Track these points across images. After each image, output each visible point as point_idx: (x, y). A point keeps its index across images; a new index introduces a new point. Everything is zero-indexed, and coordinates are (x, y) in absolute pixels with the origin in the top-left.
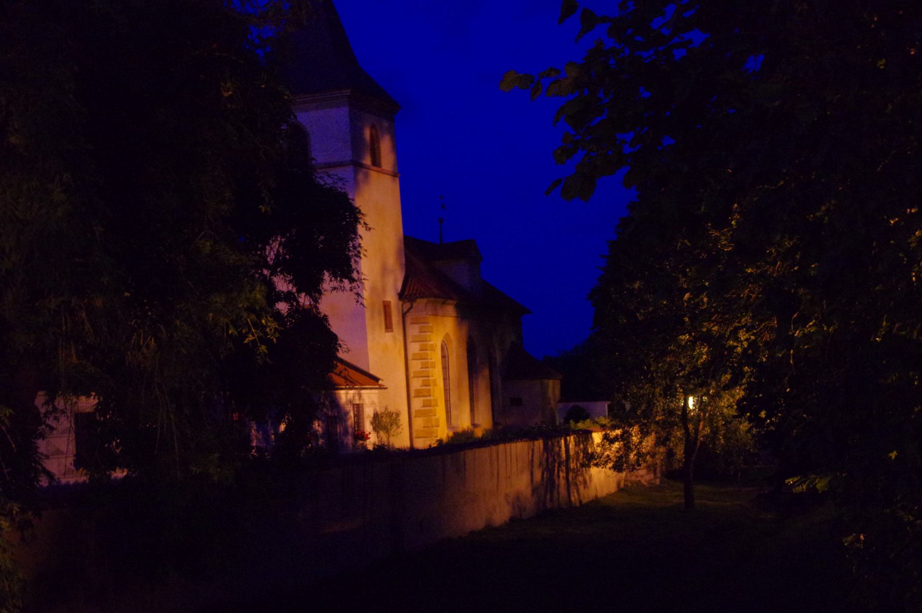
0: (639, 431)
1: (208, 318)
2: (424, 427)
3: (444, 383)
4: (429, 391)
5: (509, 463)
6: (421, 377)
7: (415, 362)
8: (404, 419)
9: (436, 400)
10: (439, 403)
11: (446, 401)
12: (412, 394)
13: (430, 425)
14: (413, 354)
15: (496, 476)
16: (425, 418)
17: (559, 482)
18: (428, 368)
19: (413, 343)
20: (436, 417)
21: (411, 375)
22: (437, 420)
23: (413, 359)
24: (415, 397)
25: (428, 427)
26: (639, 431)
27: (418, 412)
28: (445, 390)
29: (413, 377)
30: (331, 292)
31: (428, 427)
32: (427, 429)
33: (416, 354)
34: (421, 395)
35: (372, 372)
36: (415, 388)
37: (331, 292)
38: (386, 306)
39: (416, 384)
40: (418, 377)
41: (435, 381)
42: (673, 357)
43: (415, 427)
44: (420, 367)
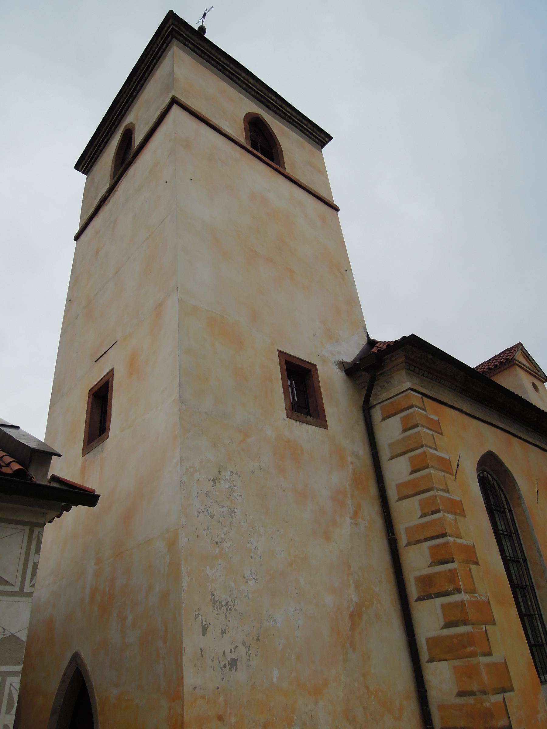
0: (356, 602)
1: (450, 551)
2: (461, 694)
4: (452, 576)
6: (426, 540)
7: (405, 503)
10: (497, 612)
12: (413, 591)
13: (475, 687)
14: (398, 486)
16: (457, 663)
18: (437, 511)
19: (392, 461)
20: (495, 658)
23: (400, 499)
24: (419, 599)
25: (471, 694)
26: (356, 602)
27: (433, 642)
29: (409, 544)
31: (471, 694)
32: (470, 700)
33: (406, 484)
34: (433, 590)
36: (418, 574)
40: (418, 542)
44: (419, 514)
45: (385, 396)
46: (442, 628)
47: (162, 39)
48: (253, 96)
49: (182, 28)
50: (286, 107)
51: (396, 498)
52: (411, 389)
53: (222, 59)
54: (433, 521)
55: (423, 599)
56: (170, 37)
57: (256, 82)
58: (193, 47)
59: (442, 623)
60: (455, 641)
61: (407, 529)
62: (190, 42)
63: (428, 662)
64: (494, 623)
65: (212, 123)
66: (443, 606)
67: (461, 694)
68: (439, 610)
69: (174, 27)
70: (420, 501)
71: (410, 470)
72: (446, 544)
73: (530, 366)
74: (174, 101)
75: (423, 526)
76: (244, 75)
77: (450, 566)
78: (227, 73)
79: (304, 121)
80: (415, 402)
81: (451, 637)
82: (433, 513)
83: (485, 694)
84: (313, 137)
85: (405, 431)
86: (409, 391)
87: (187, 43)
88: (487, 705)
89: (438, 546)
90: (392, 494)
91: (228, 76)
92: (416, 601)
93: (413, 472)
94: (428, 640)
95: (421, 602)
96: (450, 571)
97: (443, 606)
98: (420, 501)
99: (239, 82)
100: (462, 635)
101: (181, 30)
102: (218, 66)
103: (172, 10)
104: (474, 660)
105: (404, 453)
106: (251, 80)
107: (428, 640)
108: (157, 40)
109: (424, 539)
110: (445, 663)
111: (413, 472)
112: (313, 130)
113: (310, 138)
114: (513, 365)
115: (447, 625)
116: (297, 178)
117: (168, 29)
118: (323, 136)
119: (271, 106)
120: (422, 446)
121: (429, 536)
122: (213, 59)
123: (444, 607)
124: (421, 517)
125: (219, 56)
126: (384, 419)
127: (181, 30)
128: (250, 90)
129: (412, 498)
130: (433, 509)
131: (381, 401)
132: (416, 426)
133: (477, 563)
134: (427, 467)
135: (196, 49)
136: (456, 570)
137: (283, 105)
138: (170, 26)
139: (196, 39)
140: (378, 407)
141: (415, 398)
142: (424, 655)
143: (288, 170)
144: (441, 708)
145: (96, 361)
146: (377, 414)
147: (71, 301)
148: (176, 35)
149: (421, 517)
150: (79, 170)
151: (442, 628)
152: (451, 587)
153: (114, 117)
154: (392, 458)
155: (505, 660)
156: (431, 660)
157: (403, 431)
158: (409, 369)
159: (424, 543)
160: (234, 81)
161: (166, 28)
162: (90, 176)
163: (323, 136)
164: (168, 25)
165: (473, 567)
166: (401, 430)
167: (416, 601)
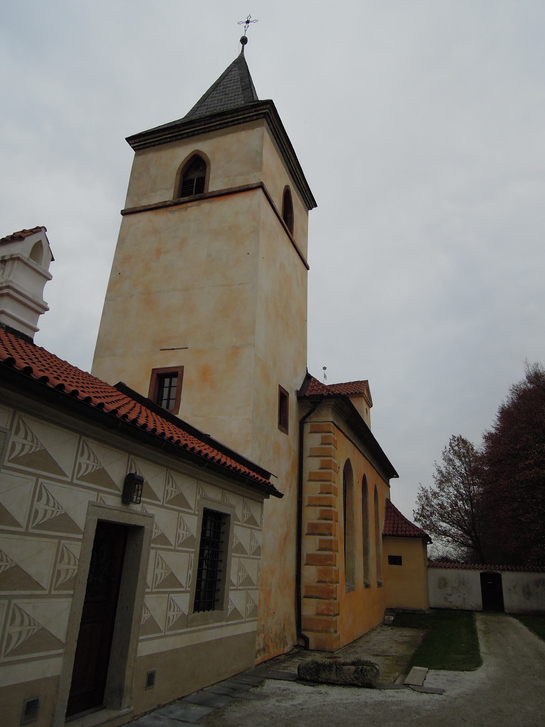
2: (319, 582)
4: (329, 527)
6: (320, 506)
7: (312, 484)
12: (305, 529)
13: (327, 579)
18: (330, 493)
19: (310, 458)
23: (309, 480)
25: (325, 582)
29: (308, 505)
31: (325, 582)
32: (324, 585)
33: (316, 474)
36: (310, 521)
40: (315, 506)
44: (319, 492)
45: (315, 419)
46: (317, 550)
47: (255, 111)
48: (289, 168)
49: (272, 114)
50: (302, 181)
51: (307, 479)
52: (332, 422)
53: (284, 140)
54: (326, 497)
55: (310, 535)
56: (262, 116)
57: (295, 160)
58: (272, 127)
59: (318, 548)
60: (322, 557)
61: (309, 497)
62: (272, 124)
63: (305, 565)
64: (338, 552)
65: (273, 204)
66: (320, 540)
67: (319, 582)
68: (318, 542)
69: (269, 111)
70: (321, 485)
71: (320, 467)
72: (330, 511)
73: (367, 396)
74: (261, 186)
75: (320, 499)
76: (290, 153)
77: (329, 522)
78: (282, 150)
79: (308, 192)
80: (332, 430)
81: (321, 555)
82: (327, 493)
83: (332, 583)
84: (307, 203)
85: (322, 444)
86: (331, 423)
87: (270, 124)
88: (331, 588)
89: (325, 511)
90: (306, 476)
91: (281, 152)
92: (306, 535)
93: (321, 469)
94: (307, 555)
95: (309, 536)
96: (329, 524)
97: (320, 540)
98: (321, 485)
99: (286, 158)
100: (327, 555)
101: (271, 114)
102: (280, 144)
103: (270, 99)
104: (330, 567)
105: (319, 456)
106: (293, 158)
107: (307, 555)
108: (250, 109)
109: (319, 505)
110: (314, 567)
111: (321, 469)
112: (309, 199)
113: (306, 203)
114: (361, 396)
115: (320, 550)
116: (301, 251)
117: (264, 109)
118: (313, 204)
119: (295, 177)
120: (330, 456)
121: (321, 504)
122: (279, 139)
123: (321, 540)
124: (320, 493)
125: (283, 138)
126: (311, 432)
127: (271, 114)
128: (289, 164)
129: (317, 482)
130: (328, 491)
131: (312, 421)
132: (330, 444)
133: (337, 522)
134: (330, 468)
135: (273, 129)
136: (332, 524)
137: (302, 179)
138: (266, 109)
139: (276, 123)
140: (309, 424)
141: (332, 428)
142: (304, 561)
143: (294, 238)
144: (307, 587)
145: (161, 350)
146: (307, 428)
147: (120, 275)
148: (267, 116)
149: (320, 493)
150: (130, 142)
151: (317, 550)
152: (327, 532)
153: (185, 130)
154: (310, 456)
155: (338, 569)
156: (306, 564)
157: (321, 444)
158: (333, 409)
159: (318, 507)
160: (283, 156)
161: (262, 108)
162: (141, 158)
163: (313, 204)
164: (264, 107)
165: (336, 523)
166: (320, 443)
167: (306, 535)
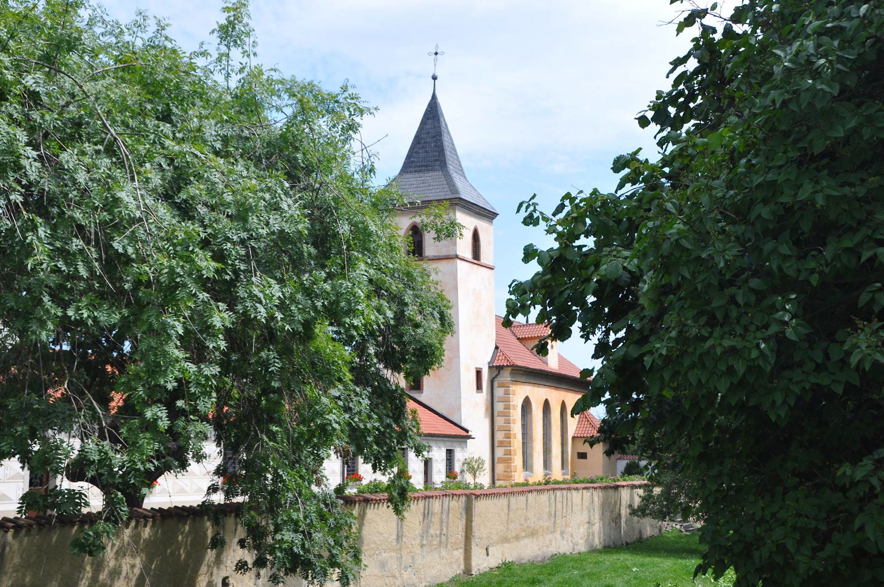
3: (523, 438)
5: (565, 505)
7: (500, 418)
8: (487, 466)
9: (515, 450)
11: (523, 452)
12: (496, 444)
15: (553, 515)
17: (360, 530)
21: (496, 428)
22: (516, 467)
23: (498, 416)
28: (523, 443)
30: (714, 7)
35: (463, 425)
37: (714, 7)
38: (479, 373)
39: (499, 436)
41: (515, 434)
42: (155, 573)
43: (497, 471)
